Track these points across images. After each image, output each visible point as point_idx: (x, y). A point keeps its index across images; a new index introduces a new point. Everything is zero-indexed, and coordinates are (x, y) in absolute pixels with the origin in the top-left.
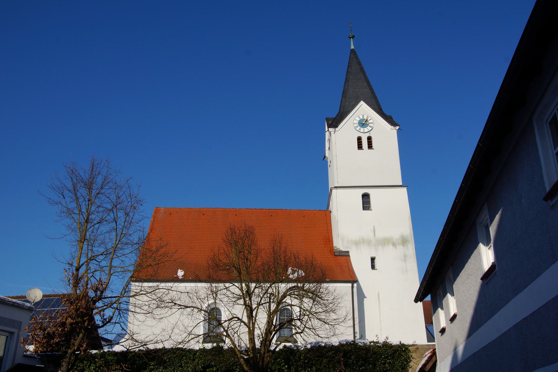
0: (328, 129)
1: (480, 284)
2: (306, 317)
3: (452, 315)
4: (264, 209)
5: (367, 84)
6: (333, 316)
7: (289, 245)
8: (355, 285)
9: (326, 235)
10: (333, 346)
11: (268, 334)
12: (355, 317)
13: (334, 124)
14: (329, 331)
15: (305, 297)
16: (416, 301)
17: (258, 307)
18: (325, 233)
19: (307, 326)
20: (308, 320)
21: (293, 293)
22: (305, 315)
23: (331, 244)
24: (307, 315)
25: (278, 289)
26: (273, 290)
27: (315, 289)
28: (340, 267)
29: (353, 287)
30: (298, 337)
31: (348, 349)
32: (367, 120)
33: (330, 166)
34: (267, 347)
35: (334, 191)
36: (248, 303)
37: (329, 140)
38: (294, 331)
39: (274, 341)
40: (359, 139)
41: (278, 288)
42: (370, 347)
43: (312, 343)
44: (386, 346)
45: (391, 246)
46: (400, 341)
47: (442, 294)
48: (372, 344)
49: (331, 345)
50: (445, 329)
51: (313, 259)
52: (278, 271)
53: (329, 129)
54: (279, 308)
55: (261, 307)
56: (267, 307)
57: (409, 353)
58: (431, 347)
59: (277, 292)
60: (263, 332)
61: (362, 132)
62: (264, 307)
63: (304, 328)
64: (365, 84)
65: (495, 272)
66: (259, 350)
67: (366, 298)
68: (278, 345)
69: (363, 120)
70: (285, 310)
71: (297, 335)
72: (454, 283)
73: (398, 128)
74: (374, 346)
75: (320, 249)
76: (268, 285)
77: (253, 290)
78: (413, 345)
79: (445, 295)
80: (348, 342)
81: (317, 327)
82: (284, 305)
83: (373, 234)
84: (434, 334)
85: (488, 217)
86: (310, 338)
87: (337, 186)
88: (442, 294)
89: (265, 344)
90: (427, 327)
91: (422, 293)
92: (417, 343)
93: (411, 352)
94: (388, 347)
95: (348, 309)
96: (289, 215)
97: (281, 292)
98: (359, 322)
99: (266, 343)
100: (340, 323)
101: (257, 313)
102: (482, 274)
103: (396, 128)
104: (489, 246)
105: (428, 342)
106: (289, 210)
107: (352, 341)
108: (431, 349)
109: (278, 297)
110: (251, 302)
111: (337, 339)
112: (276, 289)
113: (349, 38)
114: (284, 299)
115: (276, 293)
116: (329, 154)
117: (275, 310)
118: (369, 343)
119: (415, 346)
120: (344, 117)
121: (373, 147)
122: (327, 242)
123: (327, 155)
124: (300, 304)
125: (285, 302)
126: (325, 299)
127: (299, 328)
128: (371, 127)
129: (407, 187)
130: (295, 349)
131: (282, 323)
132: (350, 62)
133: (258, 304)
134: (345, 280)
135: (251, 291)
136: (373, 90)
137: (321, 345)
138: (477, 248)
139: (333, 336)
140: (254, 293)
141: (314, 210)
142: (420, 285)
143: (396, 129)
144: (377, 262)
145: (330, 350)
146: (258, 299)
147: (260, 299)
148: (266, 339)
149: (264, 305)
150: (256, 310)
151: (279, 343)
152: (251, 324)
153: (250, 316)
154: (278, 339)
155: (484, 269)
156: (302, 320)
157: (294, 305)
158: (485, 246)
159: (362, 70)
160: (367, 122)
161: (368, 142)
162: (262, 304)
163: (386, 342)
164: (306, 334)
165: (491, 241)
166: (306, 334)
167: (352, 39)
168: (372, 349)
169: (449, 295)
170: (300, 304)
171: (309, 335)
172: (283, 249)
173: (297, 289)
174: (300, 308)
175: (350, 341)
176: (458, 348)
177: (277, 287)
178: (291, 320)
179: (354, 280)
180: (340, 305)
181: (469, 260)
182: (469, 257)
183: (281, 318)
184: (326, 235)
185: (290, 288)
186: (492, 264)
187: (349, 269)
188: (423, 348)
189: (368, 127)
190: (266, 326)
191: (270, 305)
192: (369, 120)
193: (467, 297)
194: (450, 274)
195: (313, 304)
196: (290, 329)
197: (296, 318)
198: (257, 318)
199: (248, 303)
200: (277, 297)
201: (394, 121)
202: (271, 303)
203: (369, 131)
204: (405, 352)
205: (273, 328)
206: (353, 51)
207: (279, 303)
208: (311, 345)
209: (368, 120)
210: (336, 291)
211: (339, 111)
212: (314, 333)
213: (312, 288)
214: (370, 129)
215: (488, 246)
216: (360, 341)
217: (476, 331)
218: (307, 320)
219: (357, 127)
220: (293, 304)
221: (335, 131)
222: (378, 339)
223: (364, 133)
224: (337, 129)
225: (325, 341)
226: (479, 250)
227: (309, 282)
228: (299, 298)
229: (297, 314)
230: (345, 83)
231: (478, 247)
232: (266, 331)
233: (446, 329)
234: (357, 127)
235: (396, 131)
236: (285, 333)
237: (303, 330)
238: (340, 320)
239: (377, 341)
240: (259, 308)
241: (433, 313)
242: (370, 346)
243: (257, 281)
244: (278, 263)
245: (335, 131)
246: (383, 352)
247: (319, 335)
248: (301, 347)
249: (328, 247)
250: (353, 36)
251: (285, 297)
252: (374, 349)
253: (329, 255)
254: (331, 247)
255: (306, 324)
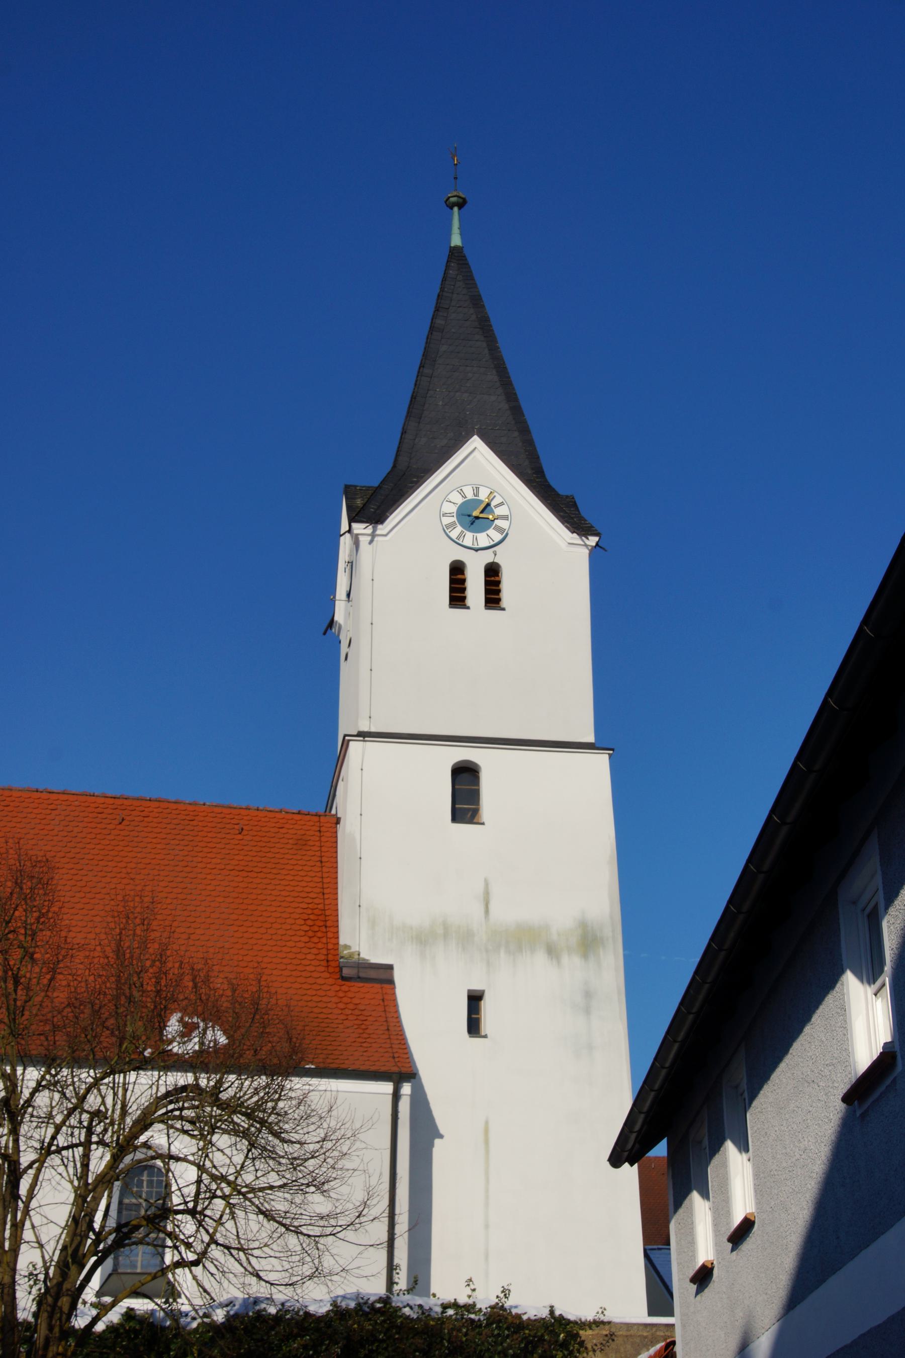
0: (350, 526)
1: (840, 1115)
2: (219, 1204)
3: (737, 1219)
4: (96, 794)
5: (496, 378)
6: (318, 1203)
7: (177, 930)
8: (406, 1089)
9: (316, 901)
10: (307, 1314)
11: (69, 1269)
12: (397, 1211)
13: (372, 508)
14: (297, 1258)
15: (219, 1128)
16: (616, 1160)
17: (41, 1161)
18: (312, 895)
19: (218, 1237)
20: (226, 1217)
21: (177, 1113)
22: (214, 1196)
23: (330, 935)
24: (224, 1197)
25: (124, 1095)
26: (103, 1098)
27: (258, 1101)
28: (356, 1022)
29: (396, 1096)
30: (183, 1278)
31: (362, 1328)
32: (488, 505)
33: (346, 659)
34: (60, 1319)
35: (355, 747)
36: (6, 1147)
37: (351, 564)
38: (169, 1257)
39: (89, 1294)
40: (457, 571)
41: (125, 1090)
42: (443, 1323)
43: (231, 1302)
44: (500, 1321)
45: (541, 959)
46: (552, 1307)
47: (706, 1142)
48: (450, 1312)
49: (301, 1313)
50: (712, 1269)
51: (260, 990)
52: (129, 1029)
53: (354, 525)
54: (122, 1166)
55: (55, 1160)
56: (74, 1161)
57: (579, 1351)
58: (658, 1333)
59: (119, 1106)
60: (52, 1260)
61: (470, 545)
62: (65, 1161)
63: (208, 1245)
64: (492, 376)
65: (888, 1081)
66: (26, 1330)
67: (441, 1137)
68: (103, 1309)
69: (475, 502)
70: (143, 1171)
71: (179, 1271)
72: (750, 1106)
73: (593, 540)
74: (456, 1320)
75: (289, 950)
76: (86, 1076)
77: (28, 1095)
78: (597, 1323)
79: (716, 1147)
80: (366, 1303)
81: (256, 1244)
82: (139, 1155)
83: (482, 909)
84: (671, 1281)
85: (878, 880)
86: (225, 1283)
87: (365, 728)
88: (706, 1142)
89: (54, 1306)
90: (652, 1256)
91: (639, 1132)
92: (611, 1315)
93: (586, 1348)
94: (508, 1328)
95: (374, 1181)
96: (186, 822)
97: (134, 1107)
98: (409, 1230)
99: (59, 1304)
100: (339, 1229)
101: (36, 1184)
102: (846, 1080)
103: (588, 542)
104: (879, 983)
105: (651, 1313)
106: (190, 804)
107: (380, 1300)
108: (658, 1342)
109: (119, 1124)
110: (16, 1141)
111: (325, 1290)
112: (115, 1094)
113: (447, 206)
114: (142, 1134)
115: (113, 1111)
116: (347, 614)
117: (107, 1174)
118: (439, 1309)
119: (601, 1326)
120: (412, 487)
121: (504, 603)
122: (316, 929)
123: (339, 617)
124: (200, 1153)
125: (146, 1145)
126: (295, 1137)
127: (188, 1246)
128: (500, 530)
129: (613, 750)
130: (168, 1323)
131: (127, 1224)
132: (445, 294)
133: (42, 1148)
134: (373, 1068)
135: (22, 1102)
136: (516, 400)
137: (265, 1310)
138: (836, 989)
139: (311, 1277)
140: (30, 1110)
141: (281, 811)
142: (635, 1105)
143: (586, 545)
144: (487, 1008)
145: (295, 1331)
146: (44, 1130)
147: (51, 1130)
148: (60, 1285)
149: (64, 1153)
150: (31, 1172)
151: (107, 1299)
152: (8, 1226)
153: (8, 1198)
154: (105, 1286)
155: (855, 1063)
156: (201, 1213)
157: (178, 1159)
158: (862, 981)
159: (485, 326)
160: (489, 513)
161: (487, 583)
162: (59, 1151)
163: (502, 1308)
164: (213, 1270)
165: (886, 969)
166: (213, 1270)
167: (456, 209)
168: (450, 1333)
169: (730, 1147)
170: (200, 1153)
171: (223, 1272)
172: (153, 948)
173: (193, 1099)
174: (201, 1168)
175: (372, 1299)
176: (752, 1346)
177: (120, 1089)
178: (166, 1212)
179: (404, 1070)
180: (345, 1163)
181: (807, 1029)
182: (806, 1018)
183: (126, 1201)
184: (316, 901)
185: (168, 1094)
186: (883, 1048)
187: (388, 1030)
188: (631, 1336)
189: (491, 532)
190: (63, 1236)
191: (86, 1157)
192: (496, 506)
193: (794, 1160)
194: (740, 1074)
195: (247, 1157)
196: (155, 1246)
197: (181, 1207)
198: (34, 1204)
199: (6, 1147)
200: (116, 1127)
201: (581, 518)
202: (94, 1147)
203: (492, 543)
204: (567, 1349)
205: (89, 1241)
206: (456, 256)
207: (122, 1149)
208: (228, 1312)
209: (493, 504)
210: (334, 1113)
211: (394, 466)
212: (245, 1268)
213: (248, 1099)
214: (497, 537)
215: (874, 983)
216: (407, 1298)
217: (817, 1288)
218: (221, 1216)
219: (452, 526)
220: (174, 1150)
221: (373, 535)
222: (474, 1294)
223: (477, 550)
224: (382, 529)
225: (280, 1295)
226: (843, 995)
227: (239, 1070)
228: (196, 1133)
229: (186, 1191)
230: (422, 366)
231: (838, 985)
232: (64, 1253)
233: (715, 1272)
234: (452, 526)
235: (587, 552)
236: (137, 1261)
237: (204, 1254)
238: (342, 1221)
239: (470, 1301)
240: (46, 1165)
241: (671, 1207)
242: (442, 1321)
243: (49, 1061)
244: (130, 999)
245: (373, 535)
246: (489, 1344)
247: (261, 1274)
248: (189, 1319)
249: (320, 946)
250: (461, 200)
251: (146, 1128)
252: (455, 1333)
253: (322, 975)
254: (330, 946)
255: (216, 1230)
